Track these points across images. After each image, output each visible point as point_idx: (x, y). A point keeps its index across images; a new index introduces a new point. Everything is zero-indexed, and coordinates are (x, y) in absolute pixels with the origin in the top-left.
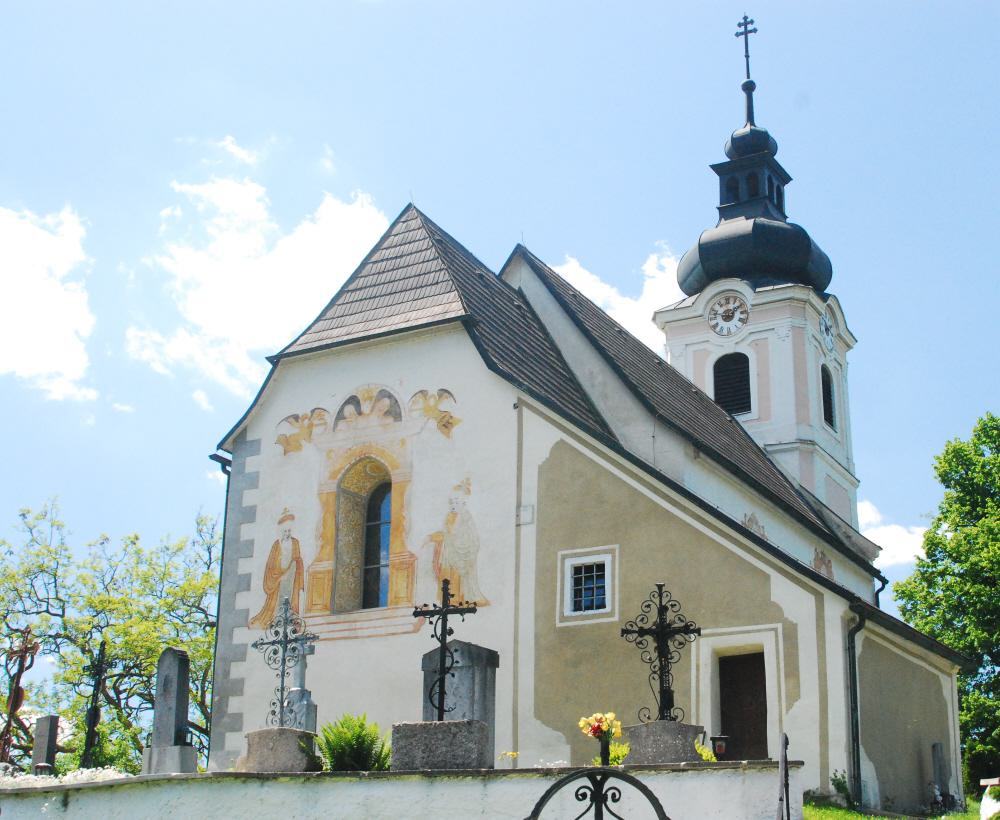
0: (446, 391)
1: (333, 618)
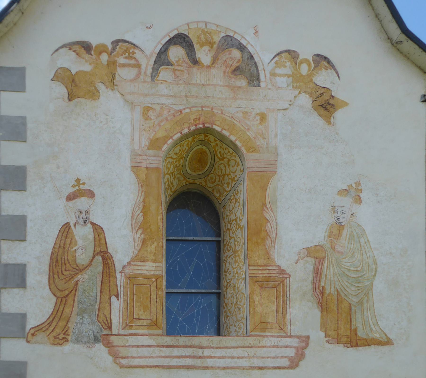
0: (325, 58)
1: (168, 340)
